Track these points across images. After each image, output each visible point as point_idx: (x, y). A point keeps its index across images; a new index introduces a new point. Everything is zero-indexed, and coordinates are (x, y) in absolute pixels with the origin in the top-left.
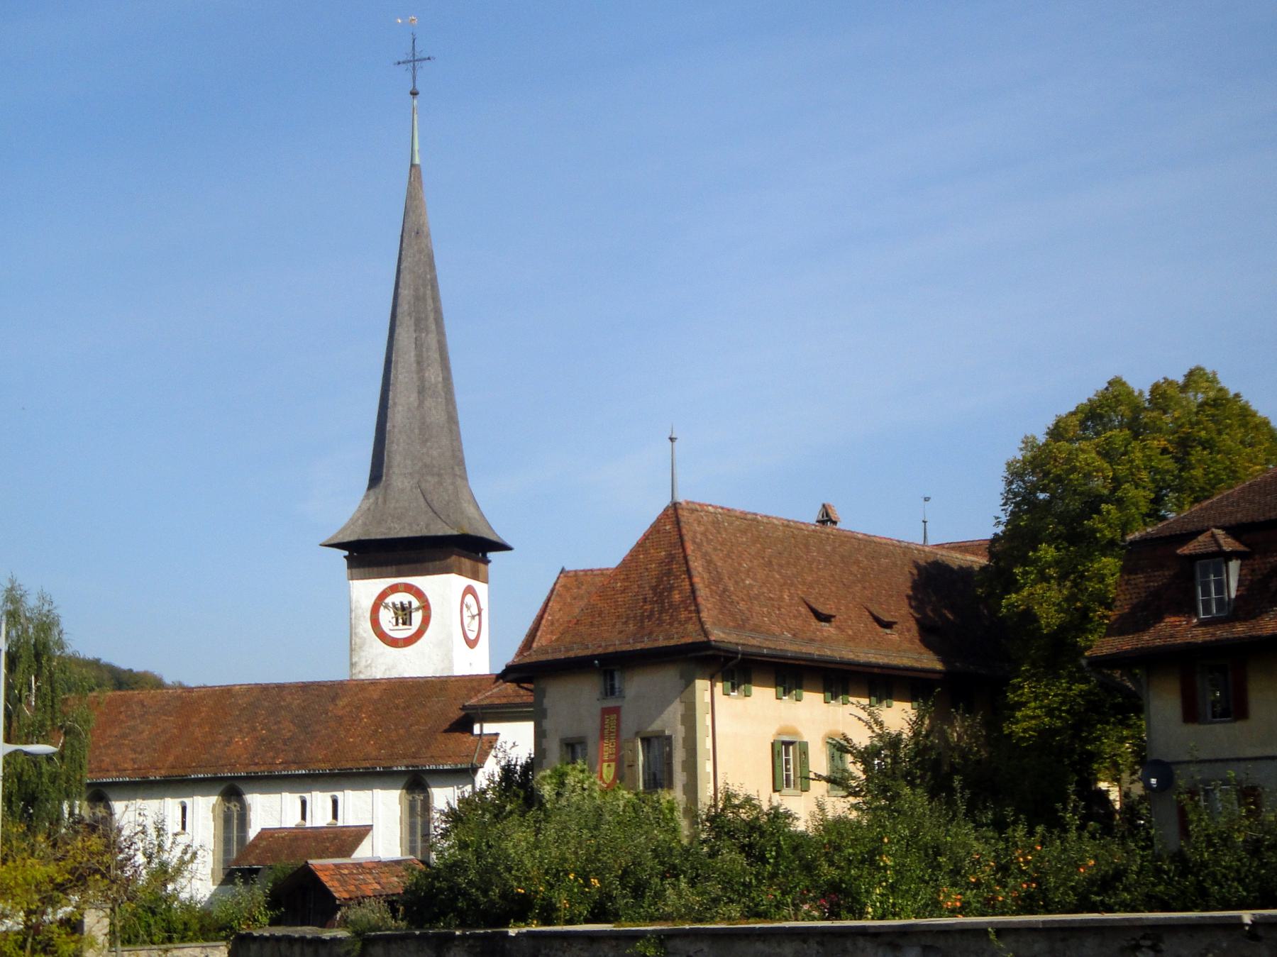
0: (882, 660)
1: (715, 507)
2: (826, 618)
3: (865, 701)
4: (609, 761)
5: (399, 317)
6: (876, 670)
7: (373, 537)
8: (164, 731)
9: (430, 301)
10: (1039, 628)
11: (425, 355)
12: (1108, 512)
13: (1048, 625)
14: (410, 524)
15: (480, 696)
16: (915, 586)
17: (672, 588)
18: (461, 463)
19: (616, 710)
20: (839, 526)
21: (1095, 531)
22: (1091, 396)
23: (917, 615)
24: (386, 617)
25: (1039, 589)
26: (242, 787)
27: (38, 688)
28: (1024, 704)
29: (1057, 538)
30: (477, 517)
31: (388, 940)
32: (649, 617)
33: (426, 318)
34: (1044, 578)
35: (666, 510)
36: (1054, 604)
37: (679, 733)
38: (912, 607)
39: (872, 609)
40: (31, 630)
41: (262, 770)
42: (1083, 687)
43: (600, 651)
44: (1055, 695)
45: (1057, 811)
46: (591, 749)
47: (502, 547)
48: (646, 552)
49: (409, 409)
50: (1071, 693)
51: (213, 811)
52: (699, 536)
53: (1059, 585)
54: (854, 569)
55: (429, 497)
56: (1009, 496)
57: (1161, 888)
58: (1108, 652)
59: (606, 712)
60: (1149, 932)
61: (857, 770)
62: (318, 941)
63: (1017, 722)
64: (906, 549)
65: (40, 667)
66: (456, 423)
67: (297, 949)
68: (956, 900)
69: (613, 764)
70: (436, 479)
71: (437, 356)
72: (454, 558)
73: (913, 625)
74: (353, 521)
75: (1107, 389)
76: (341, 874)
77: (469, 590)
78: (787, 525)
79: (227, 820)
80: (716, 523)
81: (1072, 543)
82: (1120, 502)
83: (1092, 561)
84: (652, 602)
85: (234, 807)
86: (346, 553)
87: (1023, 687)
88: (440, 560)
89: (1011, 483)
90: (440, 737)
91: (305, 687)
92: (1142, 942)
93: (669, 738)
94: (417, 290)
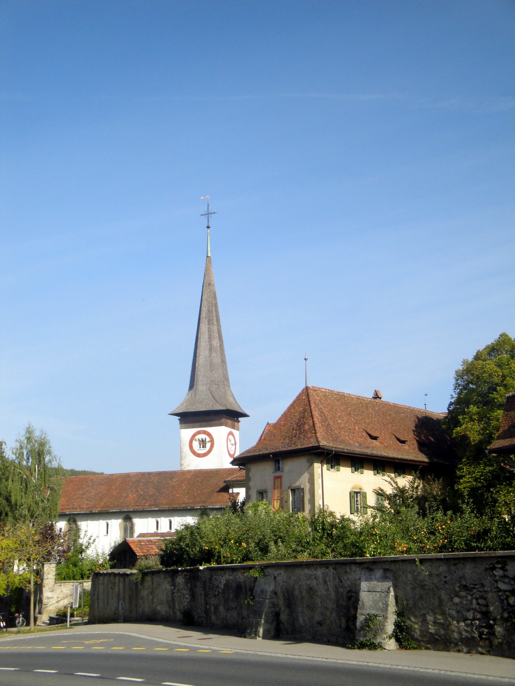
0: (400, 456)
1: (326, 390)
2: (375, 438)
3: (393, 475)
4: (277, 500)
5: (201, 319)
6: (397, 461)
7: (190, 411)
8: (100, 492)
9: (214, 312)
10: (470, 442)
11: (212, 334)
12: (500, 390)
13: (474, 441)
14: (205, 405)
15: (232, 477)
16: (416, 427)
17: (305, 423)
18: (227, 379)
19: (280, 477)
20: (382, 399)
21: (494, 399)
22: (493, 342)
23: (417, 439)
24: (196, 445)
25: (469, 425)
26: (131, 515)
27: (39, 470)
28: (464, 476)
29: (477, 403)
30: (234, 402)
31: (153, 573)
32: (295, 436)
34: (472, 420)
35: (303, 390)
36: (477, 431)
37: (307, 487)
38: (414, 435)
39: (396, 435)
40: (36, 445)
41: (140, 508)
42: (491, 468)
43: (273, 451)
44: (478, 472)
45: (459, 504)
46: (269, 495)
47: (244, 415)
48: (294, 408)
49: (206, 357)
50: (485, 471)
52: (317, 401)
53: (479, 423)
54: (388, 418)
56: (457, 385)
57: (510, 539)
58: (498, 447)
59: (276, 478)
60: (500, 560)
61: (386, 503)
62: (125, 575)
63: (461, 484)
64: (412, 410)
65: (40, 461)
66: (225, 363)
67: (117, 578)
68: (404, 547)
69: (279, 501)
70: (217, 386)
71: (217, 335)
72: (224, 419)
73: (415, 442)
74: (182, 404)
75: (499, 338)
76: (141, 545)
77: (231, 433)
78: (358, 398)
79: (125, 530)
80: (325, 396)
81: (484, 405)
82: (505, 386)
83: (493, 412)
84: (296, 430)
85: (129, 524)
86: (179, 418)
87: (463, 469)
88: (218, 420)
89: (458, 380)
90: (216, 494)
91: (160, 474)
92: (496, 566)
93: (303, 489)
94: (209, 307)
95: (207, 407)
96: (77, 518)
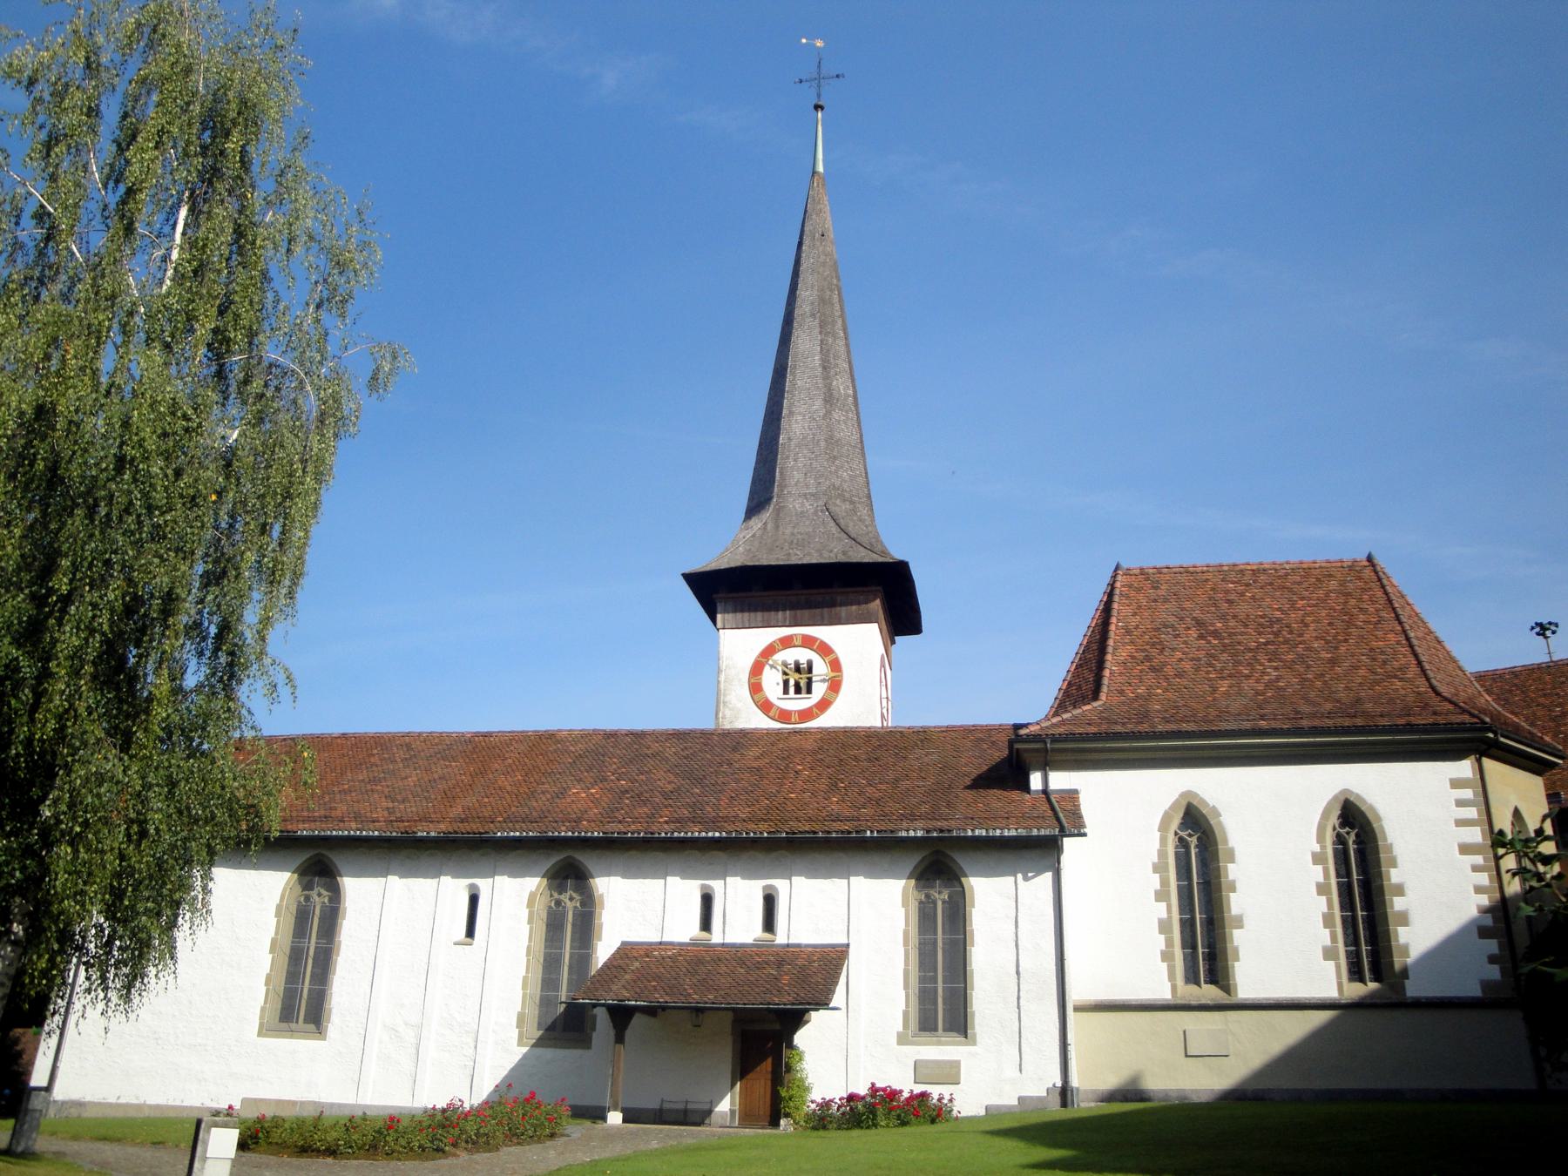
9: (837, 307)
24: (772, 681)
26: (587, 860)
33: (834, 323)
41: (635, 830)
51: (530, 903)
55: (842, 523)
70: (848, 506)
79: (554, 925)
88: (859, 603)
90: (970, 795)
95: (826, 554)
96: (338, 859)
